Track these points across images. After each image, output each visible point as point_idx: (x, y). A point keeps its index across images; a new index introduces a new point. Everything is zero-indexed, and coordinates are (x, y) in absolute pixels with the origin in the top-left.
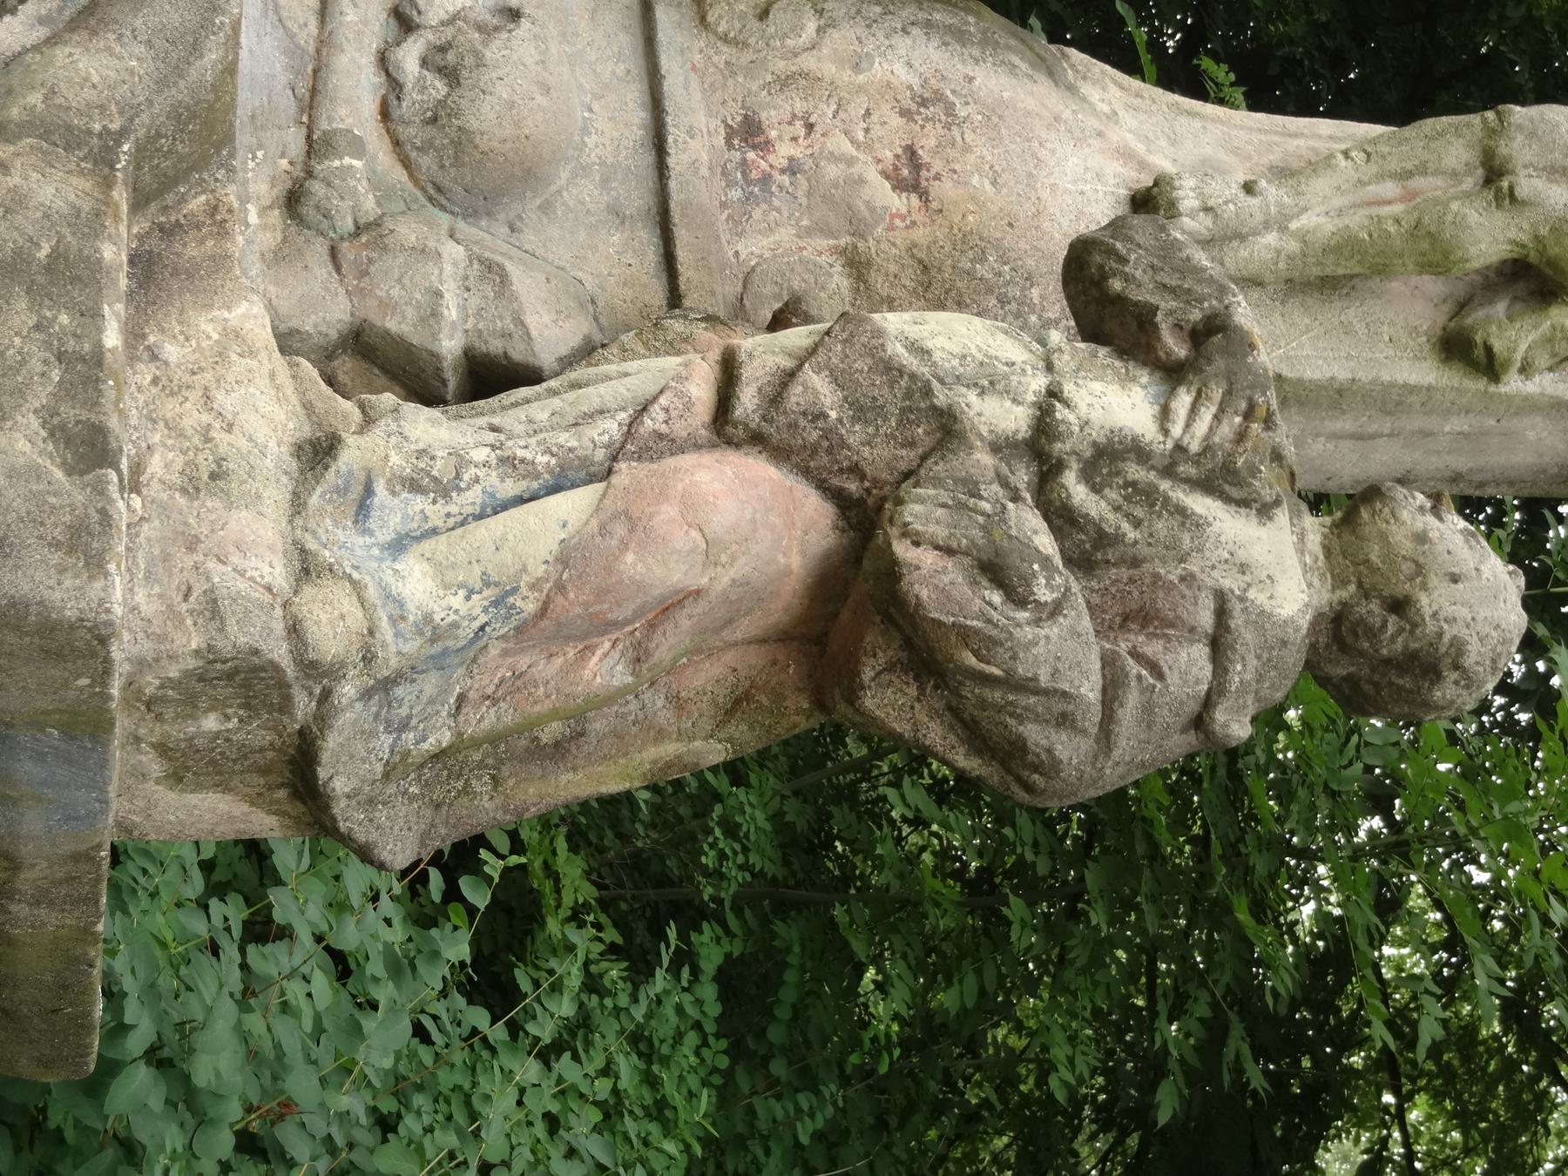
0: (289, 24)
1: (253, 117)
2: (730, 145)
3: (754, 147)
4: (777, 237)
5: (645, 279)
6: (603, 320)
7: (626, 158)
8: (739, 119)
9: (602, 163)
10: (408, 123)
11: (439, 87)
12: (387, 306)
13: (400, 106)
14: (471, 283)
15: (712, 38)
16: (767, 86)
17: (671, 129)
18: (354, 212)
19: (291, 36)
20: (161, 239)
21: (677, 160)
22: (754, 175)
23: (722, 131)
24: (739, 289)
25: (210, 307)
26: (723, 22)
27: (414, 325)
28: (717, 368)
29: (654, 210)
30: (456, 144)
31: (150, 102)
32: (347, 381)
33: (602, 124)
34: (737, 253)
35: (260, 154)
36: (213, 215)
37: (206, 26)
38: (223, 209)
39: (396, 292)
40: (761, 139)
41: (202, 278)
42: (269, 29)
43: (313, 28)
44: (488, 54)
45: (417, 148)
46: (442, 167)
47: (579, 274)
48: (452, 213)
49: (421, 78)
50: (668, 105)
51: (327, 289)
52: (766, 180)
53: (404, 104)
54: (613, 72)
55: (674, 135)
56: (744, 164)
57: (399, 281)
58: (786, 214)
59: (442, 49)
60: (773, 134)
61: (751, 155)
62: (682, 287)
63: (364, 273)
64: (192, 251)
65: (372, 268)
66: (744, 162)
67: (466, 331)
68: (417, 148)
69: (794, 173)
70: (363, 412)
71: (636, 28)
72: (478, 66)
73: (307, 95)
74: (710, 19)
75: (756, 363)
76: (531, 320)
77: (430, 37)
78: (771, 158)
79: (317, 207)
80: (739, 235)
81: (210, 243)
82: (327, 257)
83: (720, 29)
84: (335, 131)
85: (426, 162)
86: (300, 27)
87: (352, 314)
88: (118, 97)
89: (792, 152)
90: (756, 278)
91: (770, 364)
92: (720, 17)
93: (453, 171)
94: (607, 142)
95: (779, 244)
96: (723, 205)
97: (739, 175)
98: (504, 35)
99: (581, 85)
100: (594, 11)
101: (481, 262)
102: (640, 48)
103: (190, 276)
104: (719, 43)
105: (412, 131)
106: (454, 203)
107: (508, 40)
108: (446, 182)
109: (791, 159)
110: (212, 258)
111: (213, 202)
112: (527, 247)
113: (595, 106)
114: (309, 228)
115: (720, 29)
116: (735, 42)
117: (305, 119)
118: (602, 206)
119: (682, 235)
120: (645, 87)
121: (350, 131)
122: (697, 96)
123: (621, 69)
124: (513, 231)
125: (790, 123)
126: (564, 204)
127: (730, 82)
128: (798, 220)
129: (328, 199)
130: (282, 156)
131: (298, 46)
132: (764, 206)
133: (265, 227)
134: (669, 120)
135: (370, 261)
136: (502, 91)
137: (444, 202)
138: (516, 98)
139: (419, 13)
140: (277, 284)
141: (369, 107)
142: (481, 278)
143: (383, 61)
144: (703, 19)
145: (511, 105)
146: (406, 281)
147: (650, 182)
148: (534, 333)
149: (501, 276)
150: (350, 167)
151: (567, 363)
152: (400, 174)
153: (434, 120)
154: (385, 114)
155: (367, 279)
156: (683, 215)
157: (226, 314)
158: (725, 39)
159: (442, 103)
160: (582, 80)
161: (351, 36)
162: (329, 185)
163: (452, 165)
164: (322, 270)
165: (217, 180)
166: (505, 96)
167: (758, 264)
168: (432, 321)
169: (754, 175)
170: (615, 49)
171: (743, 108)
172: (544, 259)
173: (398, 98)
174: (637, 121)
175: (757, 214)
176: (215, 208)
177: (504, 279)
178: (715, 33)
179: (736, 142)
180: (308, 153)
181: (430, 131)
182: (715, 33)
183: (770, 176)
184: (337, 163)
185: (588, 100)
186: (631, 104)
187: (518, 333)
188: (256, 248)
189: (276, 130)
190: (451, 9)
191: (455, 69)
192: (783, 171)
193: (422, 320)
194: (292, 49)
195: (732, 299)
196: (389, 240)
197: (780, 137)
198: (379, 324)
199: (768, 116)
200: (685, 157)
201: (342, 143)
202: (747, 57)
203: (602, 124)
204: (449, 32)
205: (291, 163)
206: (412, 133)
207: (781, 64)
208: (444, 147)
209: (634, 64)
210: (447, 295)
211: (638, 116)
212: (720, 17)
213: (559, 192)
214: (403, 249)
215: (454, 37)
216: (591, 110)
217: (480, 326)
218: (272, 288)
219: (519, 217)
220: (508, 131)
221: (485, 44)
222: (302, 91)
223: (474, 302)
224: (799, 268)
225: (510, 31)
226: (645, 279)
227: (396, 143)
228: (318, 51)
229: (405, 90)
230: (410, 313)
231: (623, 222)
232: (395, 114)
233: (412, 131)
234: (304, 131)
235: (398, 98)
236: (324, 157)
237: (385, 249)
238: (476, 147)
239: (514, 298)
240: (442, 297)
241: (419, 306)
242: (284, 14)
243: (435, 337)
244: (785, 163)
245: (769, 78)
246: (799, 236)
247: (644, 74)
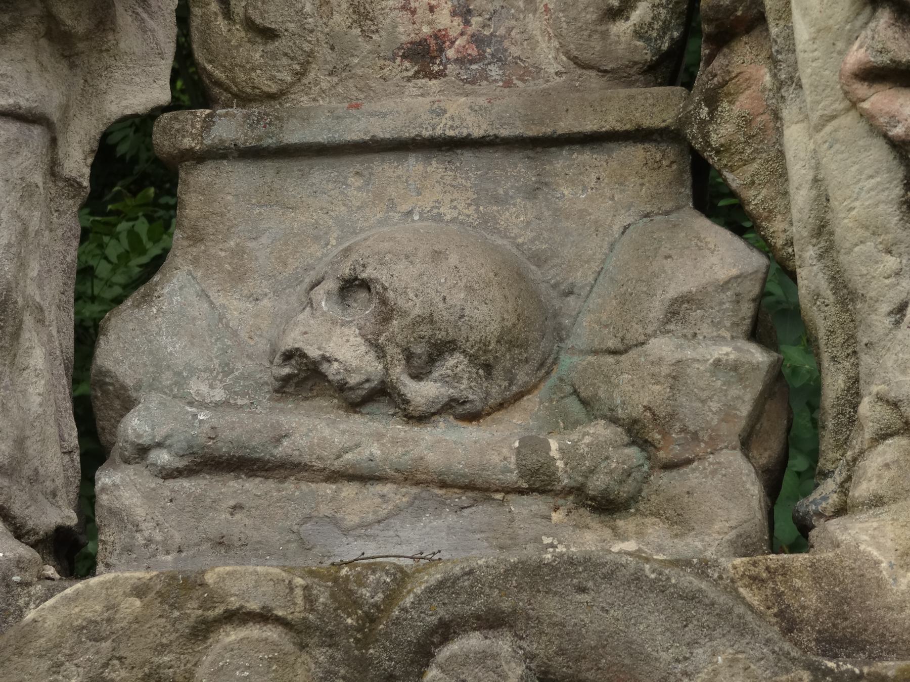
0: (383, 513)
1: (501, 548)
2: (441, 74)
3: (441, 50)
4: (537, 33)
5: (614, 165)
6: (668, 206)
7: (468, 179)
8: (407, 64)
9: (476, 203)
10: (487, 394)
11: (454, 362)
12: (727, 415)
13: (471, 402)
14: (689, 332)
15: (295, 89)
16: (366, 35)
17: (439, 132)
18: (618, 447)
19: (398, 511)
20: (800, 630)
21: (476, 128)
22: (473, 51)
23: (421, 82)
24: (593, 73)
25: (879, 582)
26: (279, 76)
27: (745, 387)
28: (877, 87)
29: (530, 153)
30: (512, 344)
31: (768, 642)
32: (766, 454)
33: (427, 201)
34: (558, 74)
35: (547, 540)
36: (763, 581)
37: (660, 587)
38: (754, 571)
39: (714, 406)
40: (432, 42)
41: (845, 590)
42: (391, 533)
43: (387, 489)
44: (417, 311)
45: (510, 385)
46: (527, 361)
47: (617, 228)
48: (558, 353)
49: (443, 379)
50: (409, 133)
51: (714, 472)
52: (478, 40)
53: (471, 397)
54: (359, 189)
55: (443, 128)
56: (461, 61)
57: (703, 402)
58: (513, 23)
59: (409, 356)
60: (426, 30)
61: (451, 53)
62: (628, 127)
63: (695, 436)
64: (812, 600)
65: (692, 428)
66: (460, 61)
67: (733, 338)
68: (510, 385)
69: (469, 12)
70: (892, 435)
71: (303, 164)
72: (432, 322)
73: (470, 494)
74: (274, 89)
75: (891, 45)
76: (722, 274)
77: (398, 370)
78: (453, 34)
79: (621, 482)
80: (539, 70)
81: (797, 583)
82: (674, 473)
83: (289, 79)
84: (519, 466)
85: (522, 377)
86: (386, 502)
87: (734, 448)
88: (768, 673)
89: (446, 12)
90: (585, 56)
91: (890, 33)
92: (272, 78)
93: (531, 350)
94: (449, 197)
95: (544, 32)
96: (508, 84)
97: (474, 67)
98: (391, 295)
99: (379, 222)
100: (285, 207)
101: (668, 321)
102: (326, 161)
103: (844, 601)
104: (305, 81)
105: (494, 390)
106: (551, 350)
107: (395, 291)
108: (538, 357)
109: (454, 14)
110: (817, 580)
111: (746, 581)
112: (591, 279)
113: (405, 208)
114: (640, 491)
115: (289, 79)
116: (305, 66)
117: (499, 496)
118: (529, 204)
119: (565, 125)
120: (377, 157)
121: (518, 451)
122: (388, 104)
123: (357, 182)
124: (571, 293)
125: (414, 12)
126: (532, 241)
127: (359, 72)
128: (518, 9)
129: (611, 472)
130: (549, 518)
131: (411, 504)
132: (506, 43)
133: (640, 535)
134: (426, 134)
135: (684, 430)
136: (458, 297)
137: (550, 360)
138: (461, 284)
139: (367, 381)
140: (712, 521)
141: (471, 433)
142: (684, 321)
143: (421, 418)
144: (271, 97)
145: (469, 289)
146: (704, 395)
147: (497, 156)
148: (734, 272)
149: (683, 302)
150: (561, 450)
151: (765, 247)
152: (531, 402)
153: (488, 368)
154: (473, 417)
155: (700, 434)
156: (542, 123)
157: (884, 565)
158: (300, 75)
159: (472, 358)
160: (373, 220)
161: (400, 450)
162: (592, 471)
163: (526, 351)
164: (692, 477)
165: (720, 577)
166: (462, 295)
167: (567, 54)
168: (742, 370)
169: (473, 51)
170: (331, 186)
171: (393, 59)
172: (603, 261)
173: (464, 402)
174: (420, 167)
175: (515, 51)
176: (754, 579)
177: (686, 299)
178: (293, 84)
179: (436, 68)
180: (542, 491)
181: (498, 372)
182: (293, 84)
183: (473, 36)
184: (560, 464)
185: (397, 216)
186: (399, 172)
187: (735, 288)
188: (667, 543)
189: (516, 524)
190: (363, 349)
191: (435, 345)
192: (467, 23)
193: (741, 380)
194: (416, 509)
195: (603, 82)
196: (662, 412)
197: (430, 23)
198: (743, 423)
199: (405, 33)
200: (471, 119)
201: (533, 460)
202: (323, 52)
203: (427, 201)
204: (391, 350)
205: (556, 509)
206: (496, 391)
207: (337, 17)
208: (512, 358)
209: (350, 168)
210: (716, 356)
211: (414, 164)
212: (272, 78)
213: (518, 246)
214: (672, 398)
215: (398, 345)
216: (410, 213)
217: (728, 324)
218: (717, 527)
219: (555, 286)
220: (495, 293)
221: (404, 314)
222: (465, 499)
223: (706, 329)
224: (573, 13)
225: (385, 289)
226: (614, 165)
227: (501, 406)
228: (417, 483)
229: (456, 395)
230: (734, 391)
231: (546, 184)
232: (479, 405)
233: (494, 390)
234: (511, 497)
235: (464, 402)
236: (552, 476)
237: (672, 416)
238: (514, 325)
239: (703, 290)
240: (719, 360)
241: (728, 383)
242: (371, 517)
243: (755, 368)
244: (458, 20)
245: (357, 31)
246: (536, 10)
247: (361, 158)
